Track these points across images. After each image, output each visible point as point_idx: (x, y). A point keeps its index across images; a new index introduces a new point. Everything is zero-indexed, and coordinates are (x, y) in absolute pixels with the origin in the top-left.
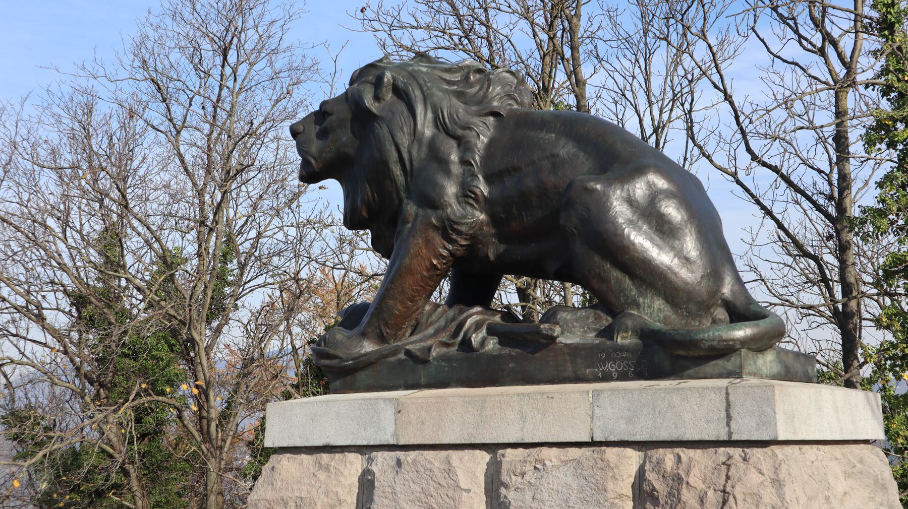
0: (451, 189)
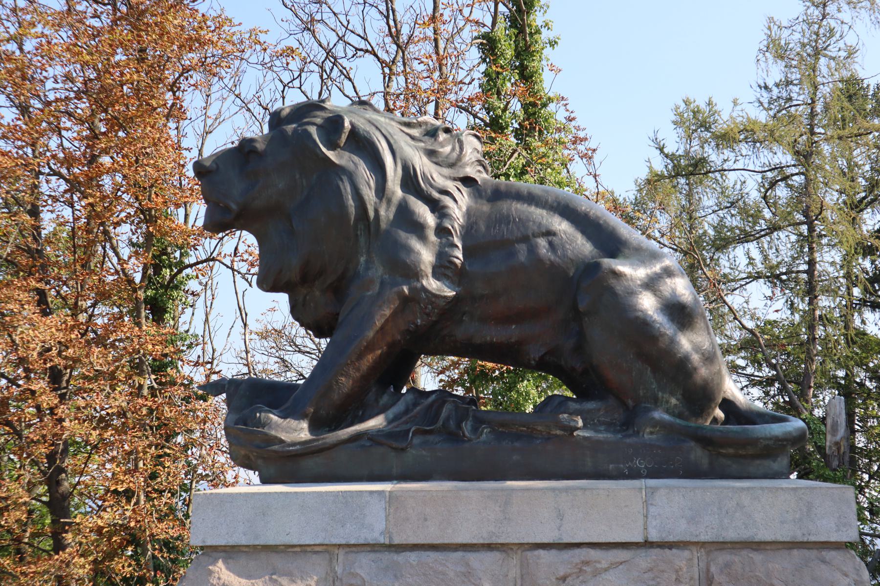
0: (426, 256)
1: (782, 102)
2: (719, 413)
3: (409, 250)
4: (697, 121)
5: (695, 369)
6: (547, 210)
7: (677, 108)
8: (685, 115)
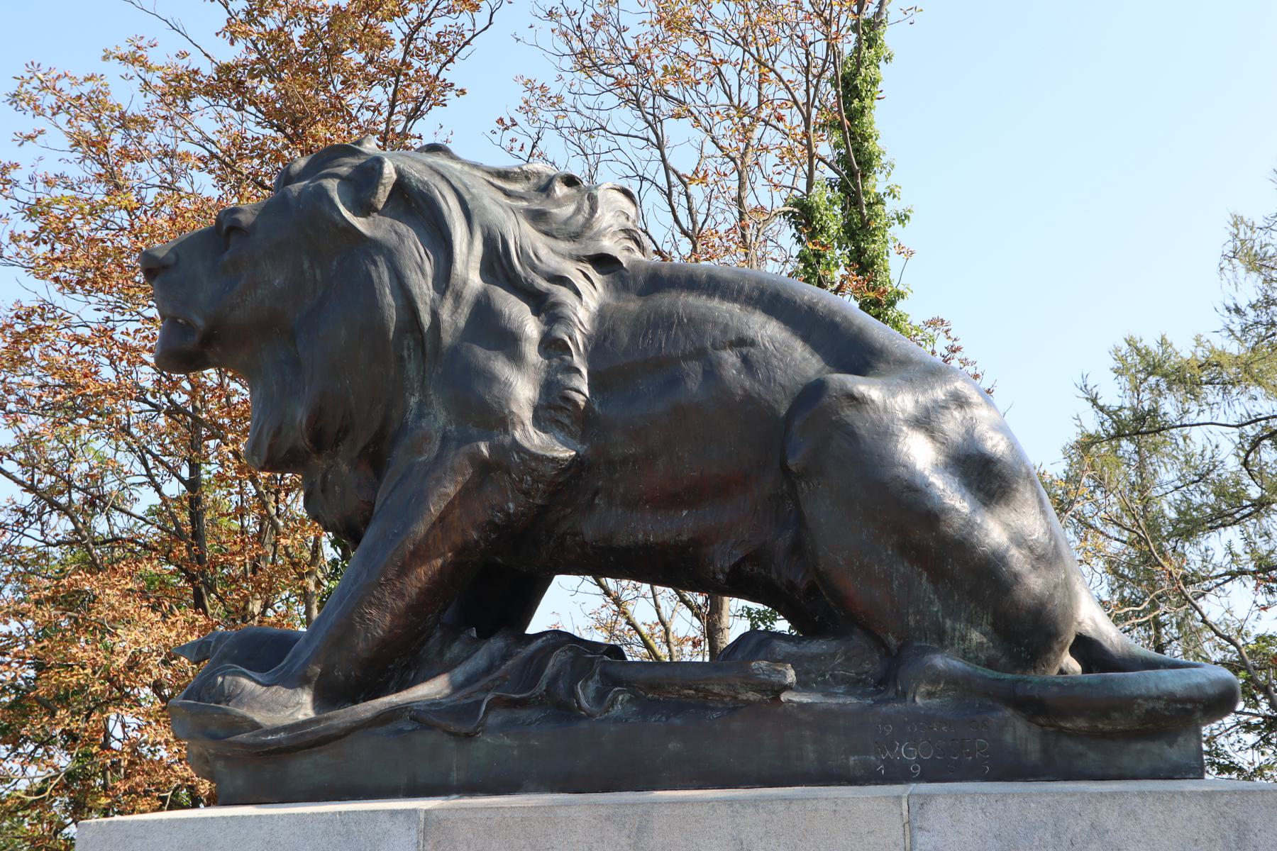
0: (523, 391)
1: (1262, 330)
2: (1071, 664)
3: (491, 379)
4: (1150, 367)
5: (1016, 576)
6: (740, 303)
7: (1117, 350)
8: (1129, 359)
